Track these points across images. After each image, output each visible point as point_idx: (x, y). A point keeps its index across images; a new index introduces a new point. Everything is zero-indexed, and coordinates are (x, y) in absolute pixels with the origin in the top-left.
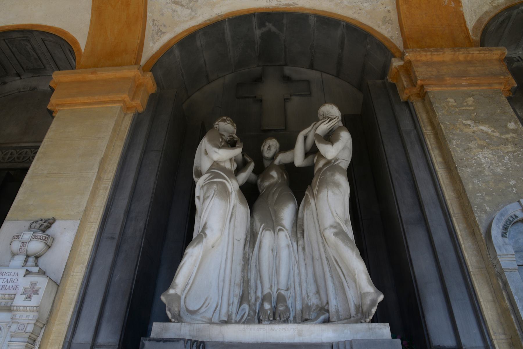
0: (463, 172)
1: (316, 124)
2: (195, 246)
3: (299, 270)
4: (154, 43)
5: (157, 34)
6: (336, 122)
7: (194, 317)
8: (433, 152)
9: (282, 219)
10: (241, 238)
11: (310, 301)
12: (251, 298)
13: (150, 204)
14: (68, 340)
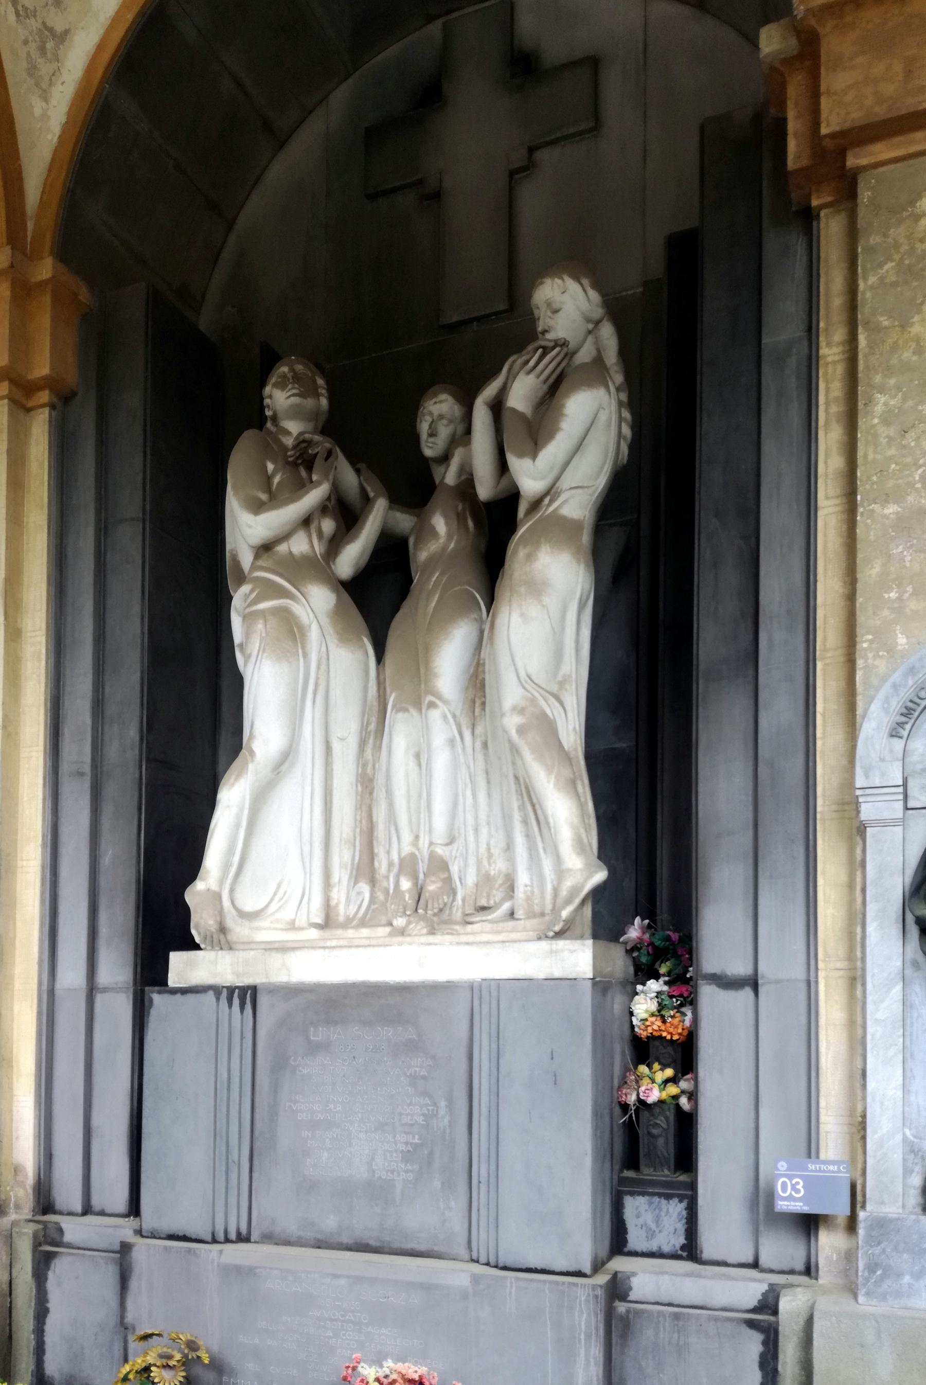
0: (869, 521)
1: (514, 362)
2: (233, 785)
3: (474, 796)
4: (45, 97)
5: (42, 50)
6: (561, 356)
7: (256, 924)
8: (826, 434)
9: (435, 675)
10: (350, 733)
11: (493, 865)
12: (380, 863)
13: (142, 678)
14: (45, 987)
